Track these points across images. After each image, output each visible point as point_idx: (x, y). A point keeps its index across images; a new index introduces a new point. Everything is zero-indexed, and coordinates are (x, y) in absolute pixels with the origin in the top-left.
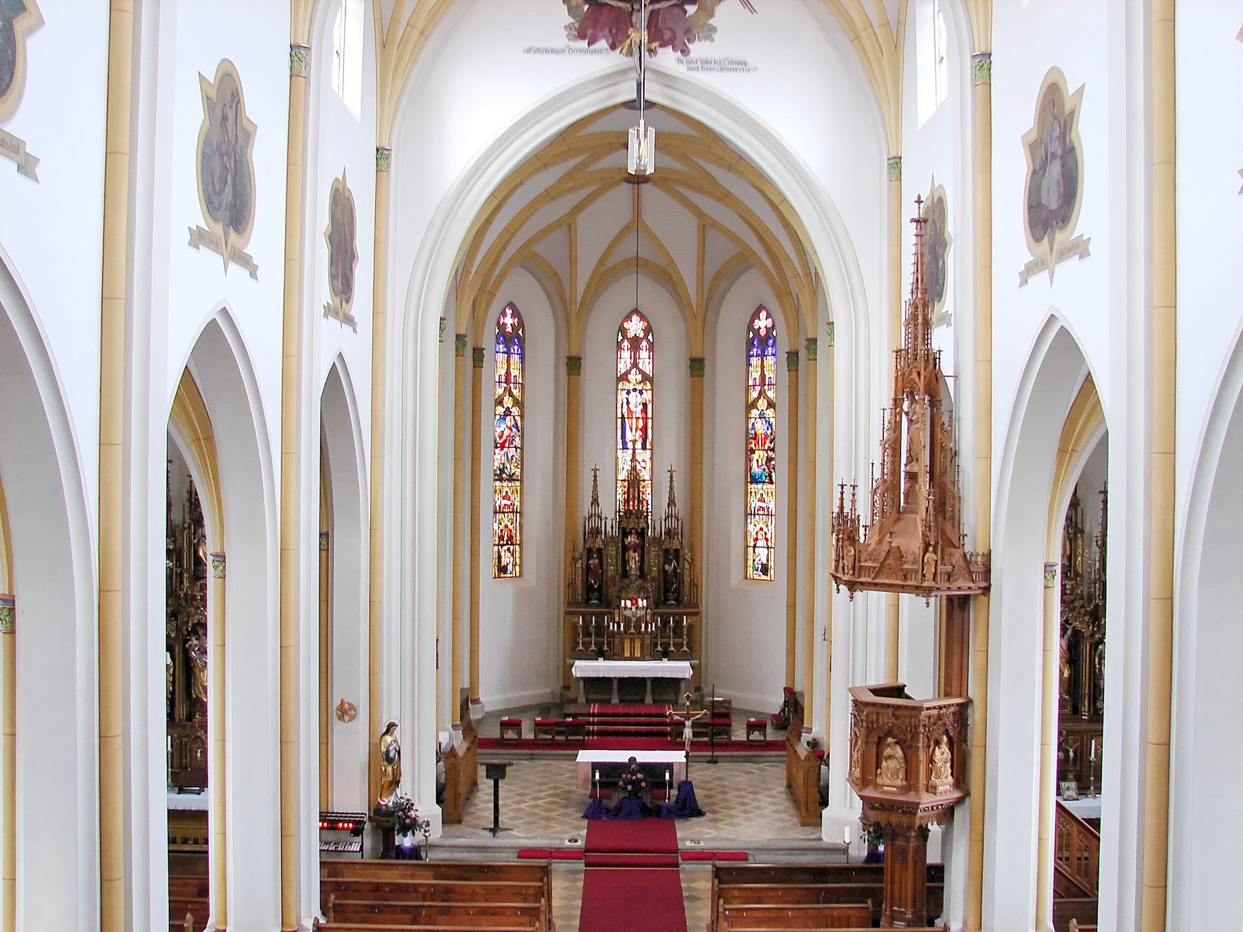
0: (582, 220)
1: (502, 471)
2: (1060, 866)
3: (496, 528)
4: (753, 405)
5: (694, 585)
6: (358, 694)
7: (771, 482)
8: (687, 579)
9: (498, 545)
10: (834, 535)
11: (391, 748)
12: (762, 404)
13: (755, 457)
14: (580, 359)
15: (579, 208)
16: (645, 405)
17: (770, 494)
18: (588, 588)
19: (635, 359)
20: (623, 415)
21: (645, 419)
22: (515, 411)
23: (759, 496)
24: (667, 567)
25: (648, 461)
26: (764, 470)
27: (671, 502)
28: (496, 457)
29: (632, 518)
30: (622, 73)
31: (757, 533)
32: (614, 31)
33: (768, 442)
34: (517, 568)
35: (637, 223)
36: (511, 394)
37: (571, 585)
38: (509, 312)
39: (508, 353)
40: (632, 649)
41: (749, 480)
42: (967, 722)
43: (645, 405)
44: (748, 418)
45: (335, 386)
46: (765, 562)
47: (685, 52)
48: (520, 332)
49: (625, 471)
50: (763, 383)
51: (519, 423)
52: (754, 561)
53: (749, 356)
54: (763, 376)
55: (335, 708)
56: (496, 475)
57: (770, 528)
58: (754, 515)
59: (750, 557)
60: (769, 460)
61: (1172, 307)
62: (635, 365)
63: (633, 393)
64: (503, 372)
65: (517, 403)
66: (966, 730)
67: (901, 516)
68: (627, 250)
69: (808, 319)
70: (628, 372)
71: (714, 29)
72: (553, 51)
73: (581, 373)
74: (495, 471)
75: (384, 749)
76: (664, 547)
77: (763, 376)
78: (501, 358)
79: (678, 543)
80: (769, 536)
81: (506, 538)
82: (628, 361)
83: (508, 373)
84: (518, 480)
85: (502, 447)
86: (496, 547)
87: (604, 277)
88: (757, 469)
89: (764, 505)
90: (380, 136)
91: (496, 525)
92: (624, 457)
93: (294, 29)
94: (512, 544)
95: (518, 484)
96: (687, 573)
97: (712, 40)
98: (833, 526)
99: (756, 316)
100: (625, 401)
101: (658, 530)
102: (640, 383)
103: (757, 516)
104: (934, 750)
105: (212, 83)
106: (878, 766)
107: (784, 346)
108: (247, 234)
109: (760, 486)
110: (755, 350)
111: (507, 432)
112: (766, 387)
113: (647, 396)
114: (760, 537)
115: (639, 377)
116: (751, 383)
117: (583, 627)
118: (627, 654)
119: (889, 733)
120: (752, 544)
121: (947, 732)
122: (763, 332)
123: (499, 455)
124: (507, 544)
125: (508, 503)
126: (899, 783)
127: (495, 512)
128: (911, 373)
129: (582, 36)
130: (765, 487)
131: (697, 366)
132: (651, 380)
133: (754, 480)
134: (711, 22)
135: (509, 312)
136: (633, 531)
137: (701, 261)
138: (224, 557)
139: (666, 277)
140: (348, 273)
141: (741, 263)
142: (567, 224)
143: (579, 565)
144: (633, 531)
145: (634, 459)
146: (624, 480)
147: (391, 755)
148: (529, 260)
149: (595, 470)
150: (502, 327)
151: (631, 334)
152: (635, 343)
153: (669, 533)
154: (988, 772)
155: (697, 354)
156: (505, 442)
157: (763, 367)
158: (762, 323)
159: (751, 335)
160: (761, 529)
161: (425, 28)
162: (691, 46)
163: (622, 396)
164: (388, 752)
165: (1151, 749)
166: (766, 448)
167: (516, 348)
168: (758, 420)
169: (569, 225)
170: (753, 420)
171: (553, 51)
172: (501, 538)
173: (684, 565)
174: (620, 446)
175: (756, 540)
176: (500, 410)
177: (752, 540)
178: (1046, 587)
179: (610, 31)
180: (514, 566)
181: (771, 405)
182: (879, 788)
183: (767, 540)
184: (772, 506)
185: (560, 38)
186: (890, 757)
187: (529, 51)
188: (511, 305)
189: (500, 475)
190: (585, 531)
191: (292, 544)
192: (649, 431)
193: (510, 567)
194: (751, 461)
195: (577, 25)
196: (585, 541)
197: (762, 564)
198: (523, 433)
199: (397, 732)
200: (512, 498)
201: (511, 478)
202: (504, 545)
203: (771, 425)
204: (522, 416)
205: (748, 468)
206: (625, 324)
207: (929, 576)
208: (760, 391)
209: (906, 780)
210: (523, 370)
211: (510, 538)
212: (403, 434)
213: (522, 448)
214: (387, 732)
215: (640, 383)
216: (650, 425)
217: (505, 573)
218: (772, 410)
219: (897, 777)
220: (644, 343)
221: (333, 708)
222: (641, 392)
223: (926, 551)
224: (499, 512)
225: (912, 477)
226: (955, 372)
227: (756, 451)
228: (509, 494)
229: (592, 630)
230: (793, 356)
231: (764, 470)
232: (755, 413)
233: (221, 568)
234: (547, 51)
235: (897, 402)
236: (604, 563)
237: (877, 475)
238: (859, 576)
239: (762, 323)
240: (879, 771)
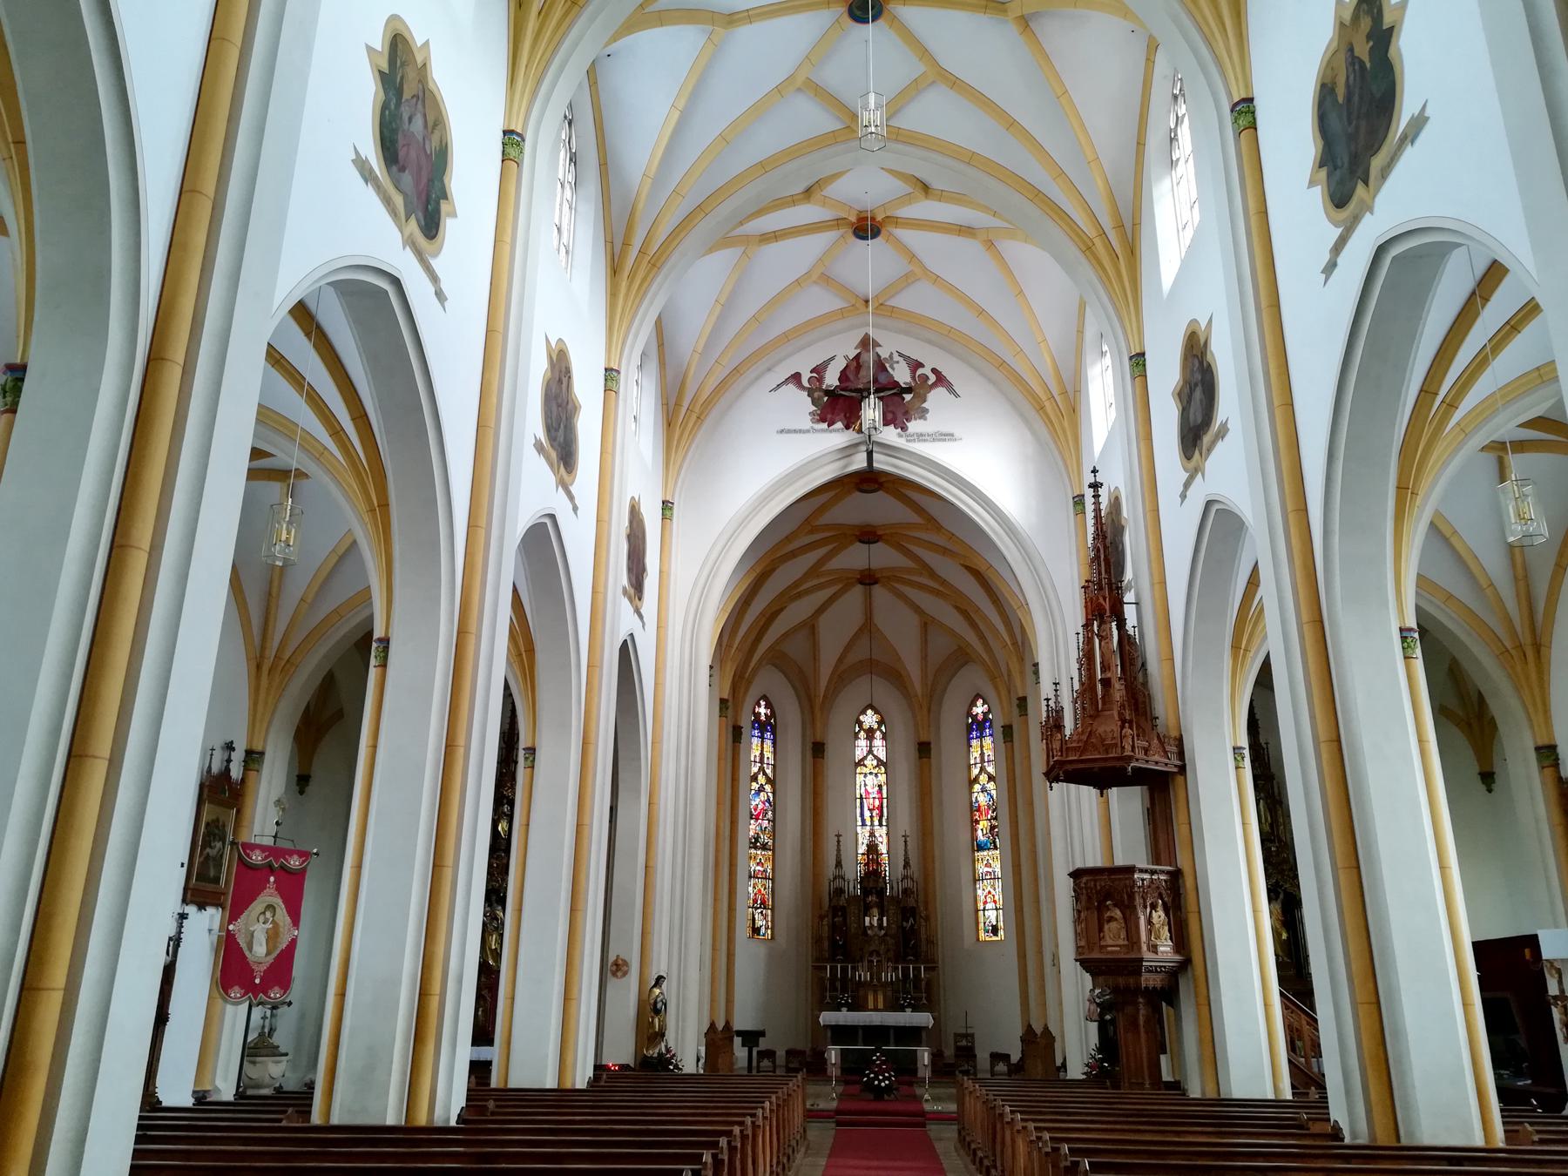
0: (823, 621)
1: (757, 840)
2: (1292, 1057)
3: (751, 889)
4: (976, 780)
5: (931, 942)
6: (627, 947)
7: (996, 848)
8: (923, 937)
9: (752, 908)
10: (1044, 741)
11: (659, 999)
12: (983, 778)
13: (980, 826)
14: (824, 744)
15: (821, 610)
16: (880, 786)
17: (995, 860)
18: (833, 942)
19: (871, 747)
20: (861, 795)
21: (881, 799)
22: (768, 788)
23: (985, 862)
24: (905, 924)
25: (884, 836)
26: (989, 838)
27: (907, 865)
28: (751, 827)
29: (872, 876)
30: (854, 446)
31: (986, 897)
32: (848, 415)
33: (990, 812)
34: (769, 931)
35: (868, 627)
36: (765, 773)
37: (817, 940)
38: (763, 703)
39: (762, 738)
40: (876, 1000)
41: (976, 848)
42: (1179, 890)
43: (880, 786)
44: (971, 793)
45: (626, 654)
46: (994, 923)
47: (904, 428)
48: (772, 721)
49: (865, 845)
50: (983, 761)
51: (771, 799)
52: (985, 923)
53: (969, 739)
54: (982, 754)
55: (609, 965)
56: (751, 843)
57: (997, 890)
58: (983, 879)
59: (981, 920)
60: (992, 828)
61: (1289, 405)
62: (870, 752)
63: (869, 777)
64: (758, 753)
65: (769, 781)
66: (1180, 898)
67: (1100, 713)
68: (860, 653)
69: (1018, 683)
70: (865, 758)
71: (926, 411)
72: (800, 431)
73: (825, 757)
74: (750, 839)
75: (652, 1001)
76: (901, 905)
77: (982, 754)
78: (756, 741)
79: (913, 901)
80: (997, 898)
81: (759, 902)
82: (865, 749)
83: (762, 754)
84: (770, 850)
85: (757, 819)
86: (750, 909)
87: (842, 678)
88: (982, 838)
89: (990, 870)
90: (666, 493)
91: (751, 889)
92: (863, 836)
93: (608, 358)
94: (765, 908)
95: (770, 853)
96: (923, 930)
97: (925, 419)
98: (1043, 733)
99: (973, 704)
100: (863, 783)
101: (895, 889)
102: (876, 767)
103: (985, 881)
104: (1151, 912)
105: (554, 347)
106: (1101, 930)
107: (998, 724)
108: (574, 472)
109: (985, 853)
110: (974, 733)
111: (760, 807)
112: (986, 764)
113: (882, 778)
114: (989, 900)
115: (875, 763)
116: (972, 762)
117: (830, 979)
118: (871, 1005)
119: (1108, 896)
120: (982, 908)
121: (1161, 896)
122: (980, 717)
123: (753, 827)
124: (760, 907)
125: (761, 869)
126: (1121, 942)
127: (750, 877)
128: (1098, 599)
129: (823, 420)
130: (990, 853)
131: (924, 749)
132: (884, 764)
133: (981, 848)
134: (924, 405)
135: (763, 703)
136: (874, 891)
137: (924, 658)
138: (534, 750)
139: (894, 675)
140: (641, 578)
141: (961, 658)
142: (810, 627)
143: (825, 922)
144: (874, 891)
145: (872, 834)
146: (863, 854)
147: (659, 1005)
148: (777, 658)
149: (838, 836)
150: (757, 715)
151: (866, 726)
152: (870, 734)
153: (905, 891)
154: (1217, 1050)
155: (924, 738)
156: (759, 814)
157: (982, 747)
158: (979, 709)
159: (970, 721)
160: (989, 892)
161: (701, 414)
162: (908, 424)
163: (860, 778)
164: (656, 1003)
165: (1324, 748)
166: (989, 817)
167: (769, 734)
168: (981, 794)
169: (813, 626)
170: (976, 794)
171: (800, 431)
172: (755, 901)
173: (920, 922)
174: (859, 823)
175: (985, 903)
176: (755, 786)
177: (982, 904)
178: (1237, 768)
179: (845, 416)
180: (767, 928)
181: (991, 778)
182: (1104, 950)
183: (995, 902)
184: (998, 870)
185: (807, 423)
186: (1111, 919)
187: (782, 431)
188: (765, 698)
189: (755, 843)
190: (830, 890)
191: (592, 736)
192: (885, 810)
193: (763, 930)
194: (976, 830)
195: (819, 412)
196: (830, 900)
197: (992, 926)
198: (774, 809)
199: (664, 986)
200: (765, 866)
201: (764, 847)
202: (758, 908)
203: (992, 797)
204: (774, 793)
205: (974, 837)
206: (861, 718)
207: (1128, 748)
208: (981, 768)
209: (1128, 940)
210: (775, 753)
211: (763, 902)
212: (679, 727)
213: (774, 821)
214: (655, 986)
215: (876, 767)
216: (885, 805)
217: (759, 934)
218: (992, 783)
219: (1119, 937)
220: (878, 733)
221: (607, 961)
222: (876, 775)
223: (1122, 727)
224: (754, 877)
225: (1106, 683)
226: (1136, 599)
227: (981, 822)
228: (763, 861)
229: (838, 985)
230: (1008, 731)
231: (989, 838)
232: (977, 787)
233: (531, 759)
234: (795, 431)
235: (1087, 625)
236: (848, 921)
237: (1077, 686)
238: (1067, 757)
239: (979, 709)
240: (1102, 935)
